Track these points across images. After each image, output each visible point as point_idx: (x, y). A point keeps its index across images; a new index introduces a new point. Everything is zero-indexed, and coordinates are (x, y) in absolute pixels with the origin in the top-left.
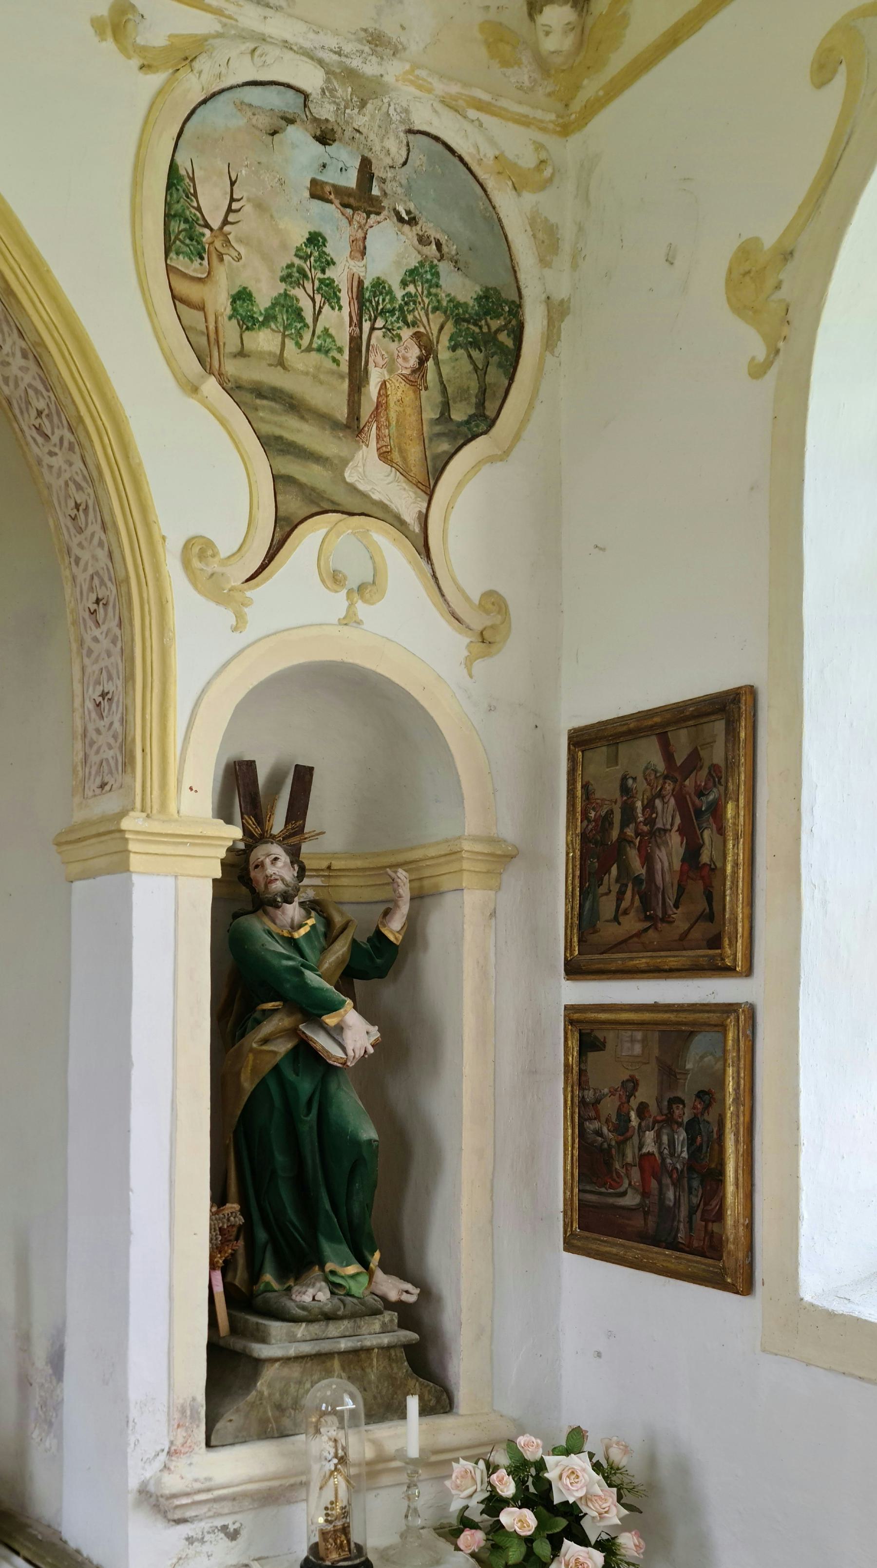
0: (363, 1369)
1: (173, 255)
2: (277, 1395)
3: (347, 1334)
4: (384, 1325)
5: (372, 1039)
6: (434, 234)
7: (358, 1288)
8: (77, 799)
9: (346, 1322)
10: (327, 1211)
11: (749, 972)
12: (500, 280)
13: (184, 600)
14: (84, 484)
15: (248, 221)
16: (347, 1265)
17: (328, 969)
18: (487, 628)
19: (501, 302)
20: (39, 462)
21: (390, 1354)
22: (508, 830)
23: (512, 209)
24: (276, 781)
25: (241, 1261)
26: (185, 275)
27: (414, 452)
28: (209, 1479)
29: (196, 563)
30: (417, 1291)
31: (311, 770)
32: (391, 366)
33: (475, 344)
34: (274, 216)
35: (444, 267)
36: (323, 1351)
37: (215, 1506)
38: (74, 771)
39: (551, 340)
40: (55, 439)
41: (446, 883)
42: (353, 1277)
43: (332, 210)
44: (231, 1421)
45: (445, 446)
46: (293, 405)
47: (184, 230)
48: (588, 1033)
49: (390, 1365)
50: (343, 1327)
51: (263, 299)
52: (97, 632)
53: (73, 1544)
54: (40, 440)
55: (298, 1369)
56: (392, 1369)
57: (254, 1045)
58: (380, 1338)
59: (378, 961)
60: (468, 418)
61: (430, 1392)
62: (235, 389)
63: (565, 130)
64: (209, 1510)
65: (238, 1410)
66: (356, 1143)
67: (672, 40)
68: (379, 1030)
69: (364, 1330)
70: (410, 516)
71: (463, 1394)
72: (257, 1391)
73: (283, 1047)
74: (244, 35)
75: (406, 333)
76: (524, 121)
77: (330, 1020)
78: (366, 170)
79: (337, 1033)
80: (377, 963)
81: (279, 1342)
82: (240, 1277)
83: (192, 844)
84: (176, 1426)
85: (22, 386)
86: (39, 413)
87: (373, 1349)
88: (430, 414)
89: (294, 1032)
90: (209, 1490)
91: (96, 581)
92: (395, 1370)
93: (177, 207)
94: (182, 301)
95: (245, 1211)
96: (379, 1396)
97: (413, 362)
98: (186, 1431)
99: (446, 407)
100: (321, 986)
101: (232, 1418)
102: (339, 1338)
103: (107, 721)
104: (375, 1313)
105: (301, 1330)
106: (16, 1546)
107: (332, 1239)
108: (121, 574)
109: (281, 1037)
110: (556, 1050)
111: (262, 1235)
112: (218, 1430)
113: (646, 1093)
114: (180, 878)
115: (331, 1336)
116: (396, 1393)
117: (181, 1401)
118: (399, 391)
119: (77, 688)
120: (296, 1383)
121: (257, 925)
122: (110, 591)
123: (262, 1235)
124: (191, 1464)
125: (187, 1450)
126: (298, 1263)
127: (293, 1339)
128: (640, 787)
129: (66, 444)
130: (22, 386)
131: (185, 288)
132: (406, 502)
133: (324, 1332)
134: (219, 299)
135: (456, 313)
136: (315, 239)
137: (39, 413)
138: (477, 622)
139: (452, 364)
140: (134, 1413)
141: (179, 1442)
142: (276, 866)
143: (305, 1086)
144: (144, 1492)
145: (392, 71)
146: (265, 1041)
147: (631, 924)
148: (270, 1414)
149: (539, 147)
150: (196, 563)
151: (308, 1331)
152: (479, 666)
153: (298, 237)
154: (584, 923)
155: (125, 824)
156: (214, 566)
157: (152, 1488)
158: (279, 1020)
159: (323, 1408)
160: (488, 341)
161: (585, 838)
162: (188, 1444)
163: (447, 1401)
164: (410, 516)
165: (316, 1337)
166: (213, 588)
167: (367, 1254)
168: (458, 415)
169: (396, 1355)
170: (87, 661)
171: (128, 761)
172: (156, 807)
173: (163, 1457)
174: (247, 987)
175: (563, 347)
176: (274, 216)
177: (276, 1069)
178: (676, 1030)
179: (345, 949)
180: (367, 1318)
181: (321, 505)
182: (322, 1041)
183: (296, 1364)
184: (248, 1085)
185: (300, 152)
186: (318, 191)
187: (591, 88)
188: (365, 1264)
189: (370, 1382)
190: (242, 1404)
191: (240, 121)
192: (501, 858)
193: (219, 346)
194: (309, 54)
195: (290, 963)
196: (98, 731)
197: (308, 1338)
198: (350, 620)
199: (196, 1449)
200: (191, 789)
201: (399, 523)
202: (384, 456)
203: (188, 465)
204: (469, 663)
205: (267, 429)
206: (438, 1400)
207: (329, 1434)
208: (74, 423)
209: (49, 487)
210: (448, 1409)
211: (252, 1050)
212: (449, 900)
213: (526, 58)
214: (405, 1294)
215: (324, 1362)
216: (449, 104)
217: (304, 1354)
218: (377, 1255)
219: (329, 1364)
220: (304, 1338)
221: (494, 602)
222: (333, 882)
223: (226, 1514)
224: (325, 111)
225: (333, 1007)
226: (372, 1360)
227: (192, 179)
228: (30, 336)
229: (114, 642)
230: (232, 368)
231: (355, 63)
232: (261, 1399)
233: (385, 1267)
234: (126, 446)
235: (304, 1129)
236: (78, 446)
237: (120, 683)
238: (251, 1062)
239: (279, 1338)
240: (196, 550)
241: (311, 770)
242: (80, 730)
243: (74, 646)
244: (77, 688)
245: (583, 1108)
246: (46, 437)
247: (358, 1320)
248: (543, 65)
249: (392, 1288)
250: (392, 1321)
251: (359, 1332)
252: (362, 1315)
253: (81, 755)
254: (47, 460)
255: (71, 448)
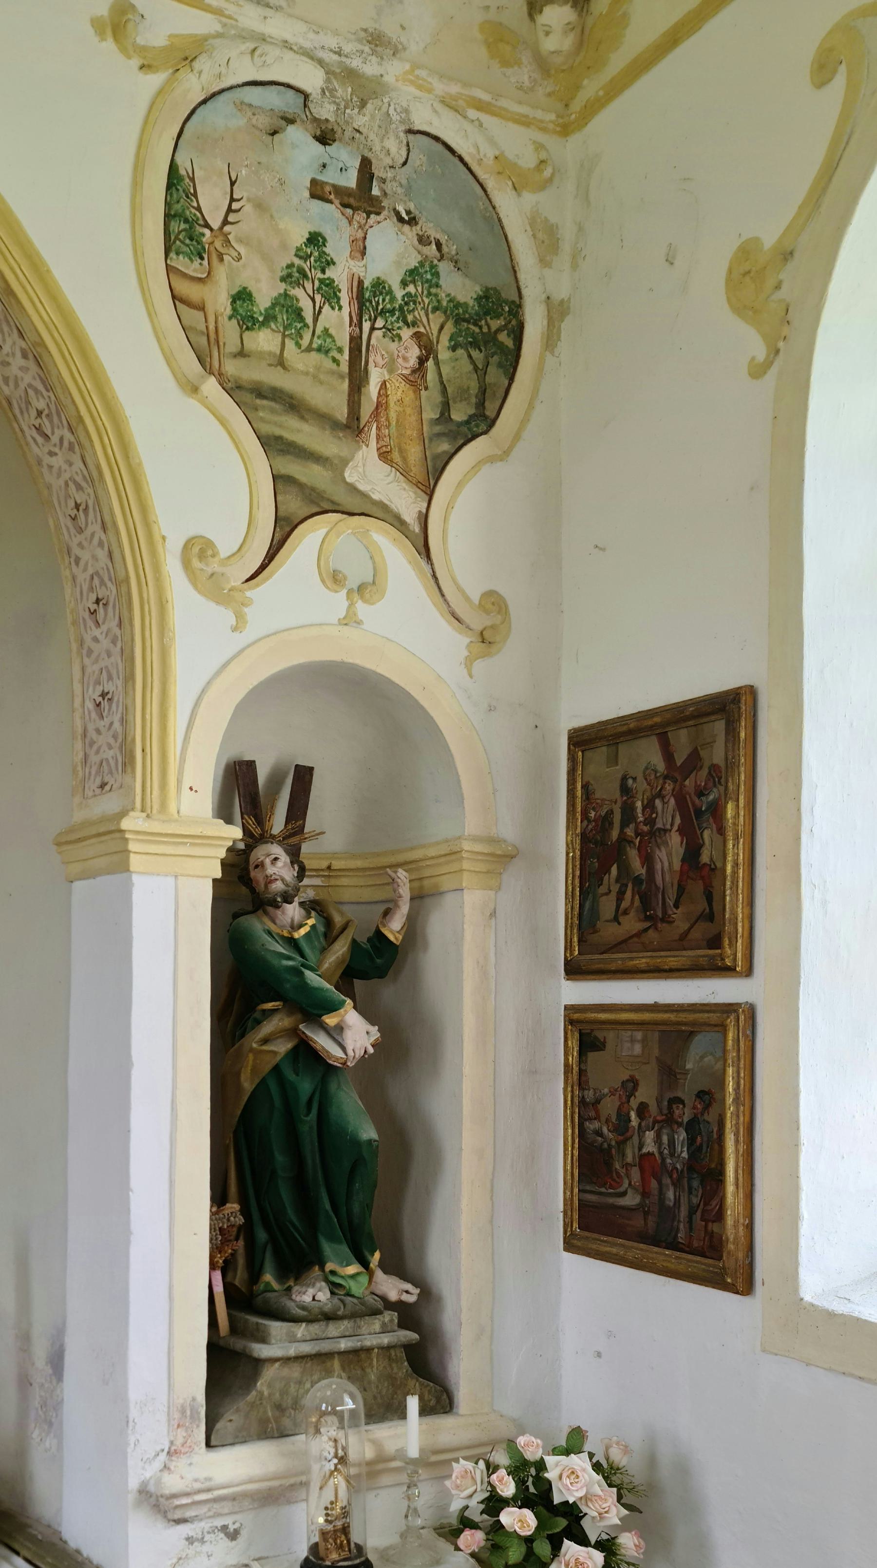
0: (363, 1369)
1: (173, 255)
2: (277, 1395)
3: (347, 1334)
4: (384, 1325)
5: (372, 1039)
6: (434, 234)
7: (358, 1288)
8: (77, 799)
9: (346, 1322)
10: (327, 1211)
11: (749, 972)
12: (500, 280)
13: (184, 600)
14: (84, 484)
15: (248, 221)
16: (347, 1265)
17: (328, 969)
18: (487, 628)
19: (501, 302)
20: (39, 462)
21: (390, 1354)
22: (508, 830)
23: (512, 209)
24: (276, 781)
25: (241, 1261)
26: (185, 275)
27: (414, 452)
28: (209, 1479)
29: (196, 563)
30: (417, 1291)
31: (311, 770)
32: (391, 366)
33: (475, 344)
34: (274, 216)
35: (444, 267)
36: (323, 1351)
37: (215, 1506)
38: (74, 771)
39: (551, 340)
40: (55, 439)
41: (446, 883)
42: (353, 1277)
43: (332, 210)
44: (231, 1421)
45: (445, 446)
46: (293, 405)
47: (184, 230)
48: (588, 1033)
49: (390, 1365)
50: (343, 1327)
51: (263, 299)
52: (97, 632)
53: (73, 1544)
54: (40, 440)
55: (298, 1369)
56: (392, 1369)
57: (254, 1045)
58: (380, 1338)
59: (378, 961)
60: (468, 418)
61: (430, 1392)
62: (235, 389)
63: (565, 130)
64: (209, 1510)
65: (238, 1410)
66: (356, 1143)
67: (672, 40)
68: (379, 1030)
69: (364, 1330)
70: (410, 516)
71: (463, 1394)
72: (257, 1391)
73: (283, 1047)
74: (244, 35)
75: (406, 333)
76: (524, 121)
77: (330, 1020)
78: (366, 170)
79: (337, 1033)
80: (377, 963)
81: (279, 1342)
82: (240, 1277)
83: (192, 844)
84: (176, 1426)
85: (22, 386)
86: (39, 413)
87: (373, 1349)
88: (430, 414)
89: (294, 1032)
90: (209, 1490)
91: (96, 581)
92: (395, 1370)
93: (177, 207)
94: (182, 301)
95: (245, 1211)
96: (379, 1396)
97: (413, 362)
98: (186, 1431)
99: (446, 407)
100: (321, 986)
101: (232, 1418)
102: (339, 1338)
103: (107, 721)
104: (375, 1313)
105: (301, 1330)
106: (16, 1546)
107: (332, 1239)
108: (121, 574)
109: (281, 1037)
110: (556, 1050)
111: (262, 1235)
112: (218, 1430)
113: (646, 1093)
114: (180, 878)
115: (331, 1336)
116: (396, 1393)
117: (181, 1401)
118: (399, 391)
119: (77, 688)
120: (296, 1383)
121: (257, 925)
122: (110, 591)
123: (262, 1235)
124: (191, 1464)
125: (187, 1450)
126: (298, 1263)
127: (293, 1339)
128: (640, 787)
129: (66, 444)
130: (22, 386)
131: (185, 288)
132: (406, 502)
133: (324, 1332)
134: (219, 299)
135: (456, 313)
136: (315, 239)
137: (39, 413)
138: (477, 622)
139: (452, 364)
140: (134, 1413)
141: (179, 1442)
142: (276, 866)
143: (305, 1086)
144: (144, 1492)
145: (392, 71)
146: (265, 1041)
147: (631, 924)
148: (270, 1414)
149: (539, 147)
150: (196, 563)
151: (308, 1331)
152: (479, 666)
153: (298, 237)
154: (584, 923)
155: (125, 824)
156: (214, 566)
157: (152, 1488)
158: (279, 1020)
159: (323, 1408)
160: (488, 341)
161: (585, 838)
162: (188, 1444)
163: (447, 1401)
164: (410, 516)
165: (316, 1337)
166: (213, 588)
167: (367, 1254)
168: (458, 415)
169: (396, 1355)
170: (87, 661)
171: (128, 761)
172: (156, 807)
173: (163, 1457)
174: (247, 987)
175: (563, 347)
176: (274, 216)
177: (276, 1069)
178: (676, 1030)
179: (345, 949)
180: (367, 1318)
181: (321, 505)
182: (322, 1041)
183: (296, 1364)
184: (248, 1085)
185: (300, 152)
186: (318, 191)
187: (591, 88)
188: (365, 1264)
189: (370, 1382)
190: (242, 1404)
191: (240, 121)
192: (501, 858)
193: (219, 346)
194: (309, 54)
195: (290, 963)
196: (98, 731)
197: (308, 1338)
198: (350, 620)
199: (196, 1449)
200: (191, 789)
201: (399, 523)
202: (384, 456)
203: (188, 465)
204: (469, 663)
205: (267, 429)
206: (438, 1400)
207: (329, 1434)
208: (74, 423)
209: (49, 487)
210: (448, 1409)
211: (252, 1050)
212: (449, 900)
213: (526, 58)
214: (405, 1294)
215: (324, 1362)
216: (449, 104)
217: (304, 1354)
218: (377, 1255)
219: (329, 1364)
220: (304, 1338)
221: (494, 602)
222: (333, 882)
223: (226, 1514)
224: (325, 111)
225: (333, 1007)
226: (372, 1360)
227: (192, 179)
228: (30, 336)
229: (114, 642)
230: (232, 368)
231: (355, 63)
232: (261, 1399)
233: (385, 1267)
234: (126, 446)
235: (304, 1129)
236: (78, 446)
237: (120, 683)
238: (251, 1062)
239: (279, 1338)
240: (196, 550)
241: (311, 770)
242: (80, 730)
243: (74, 646)
244: (77, 688)
245: (583, 1108)
246: (46, 437)
247: (358, 1320)
248: (543, 65)
249: (392, 1288)
250: (392, 1321)
251: (359, 1332)
252: (362, 1315)
253: (81, 755)
254: (47, 460)
255: (71, 448)
